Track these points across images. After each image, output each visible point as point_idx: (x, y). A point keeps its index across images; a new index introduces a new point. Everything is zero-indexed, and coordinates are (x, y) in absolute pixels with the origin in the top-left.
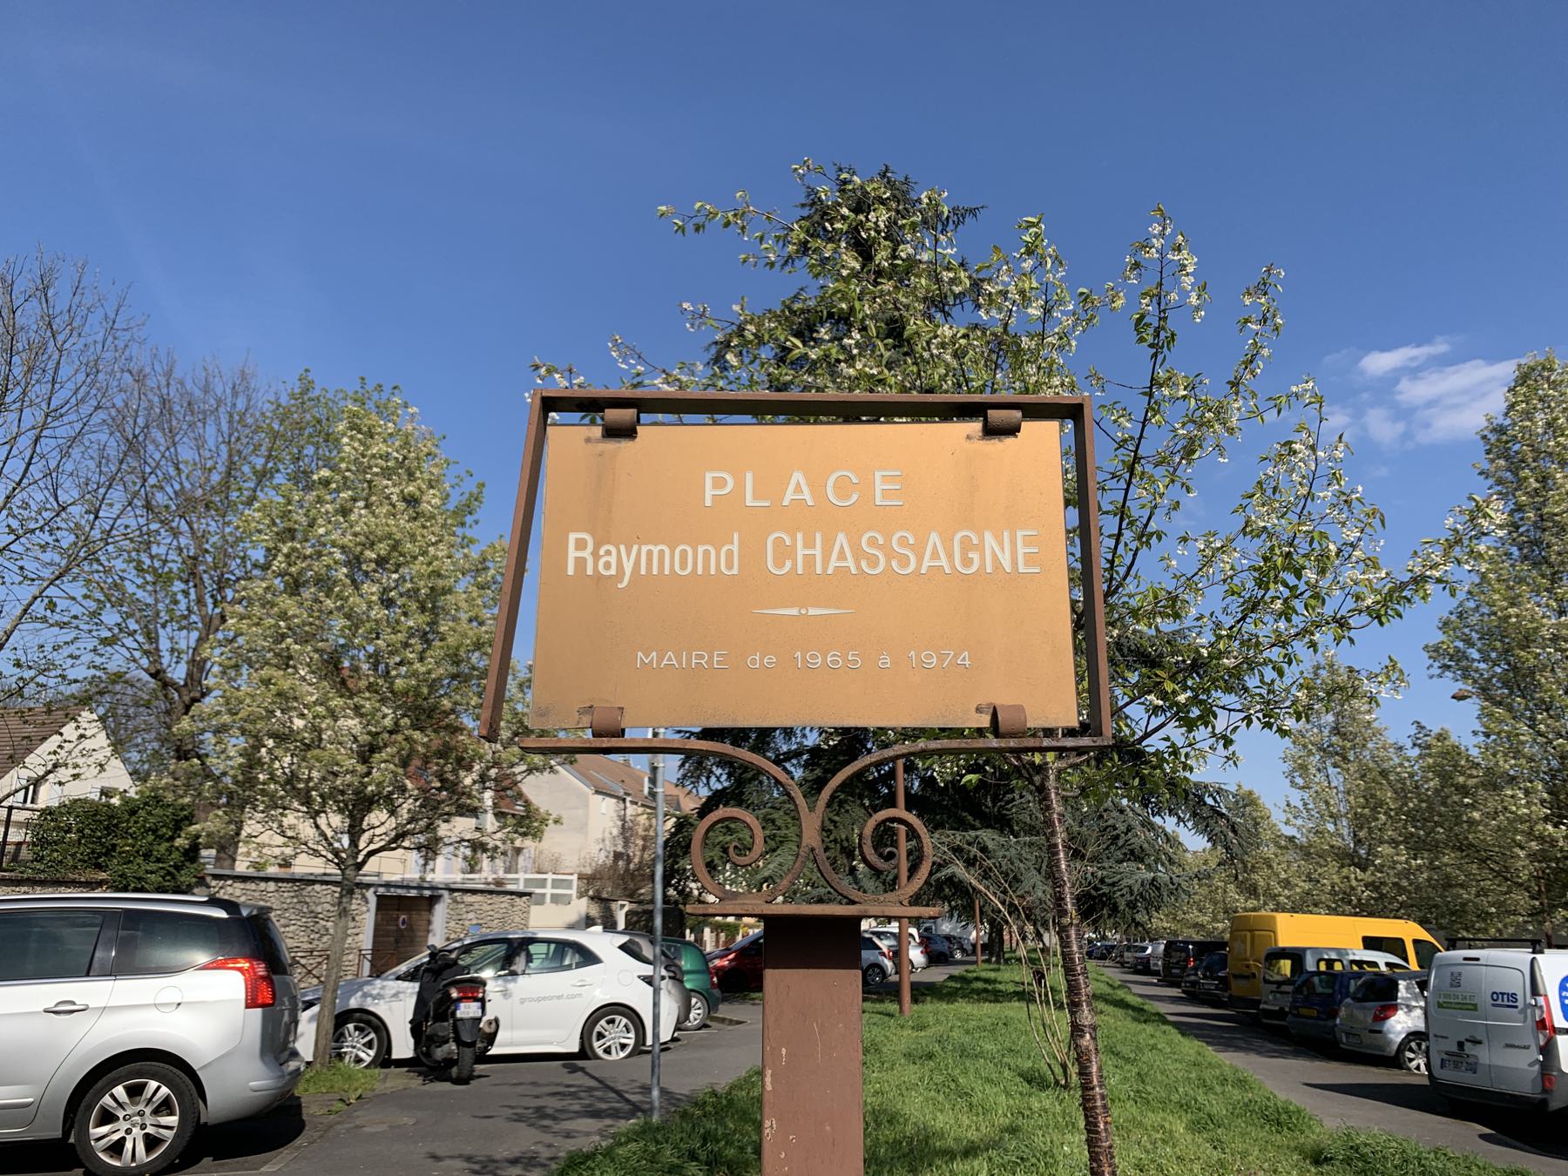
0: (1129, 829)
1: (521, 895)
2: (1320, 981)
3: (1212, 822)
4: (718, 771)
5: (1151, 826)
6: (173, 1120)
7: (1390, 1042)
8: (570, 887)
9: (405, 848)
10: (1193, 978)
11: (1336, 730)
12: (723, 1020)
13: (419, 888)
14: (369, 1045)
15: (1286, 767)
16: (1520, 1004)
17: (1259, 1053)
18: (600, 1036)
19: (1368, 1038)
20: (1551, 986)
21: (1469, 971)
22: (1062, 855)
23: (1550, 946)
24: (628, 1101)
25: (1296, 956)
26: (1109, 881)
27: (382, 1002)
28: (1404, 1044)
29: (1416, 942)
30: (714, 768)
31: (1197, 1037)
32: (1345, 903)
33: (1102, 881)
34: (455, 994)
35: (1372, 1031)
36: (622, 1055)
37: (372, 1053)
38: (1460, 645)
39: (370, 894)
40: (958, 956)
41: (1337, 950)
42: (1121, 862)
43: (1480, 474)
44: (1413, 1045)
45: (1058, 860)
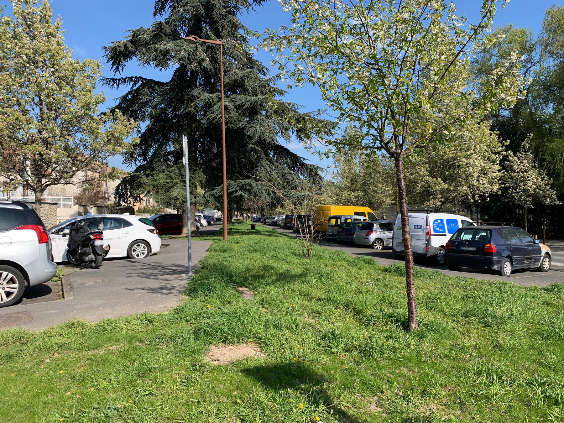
0: (294, 179)
3: (315, 177)
4: (140, 158)
6: (16, 285)
7: (370, 242)
8: (71, 201)
16: (422, 228)
17: (331, 246)
19: (364, 240)
20: (431, 223)
22: (402, 181)
25: (337, 218)
28: (374, 242)
29: (368, 213)
30: (138, 157)
32: (348, 202)
34: (92, 237)
35: (365, 238)
36: (143, 256)
40: (212, 222)
44: (377, 242)
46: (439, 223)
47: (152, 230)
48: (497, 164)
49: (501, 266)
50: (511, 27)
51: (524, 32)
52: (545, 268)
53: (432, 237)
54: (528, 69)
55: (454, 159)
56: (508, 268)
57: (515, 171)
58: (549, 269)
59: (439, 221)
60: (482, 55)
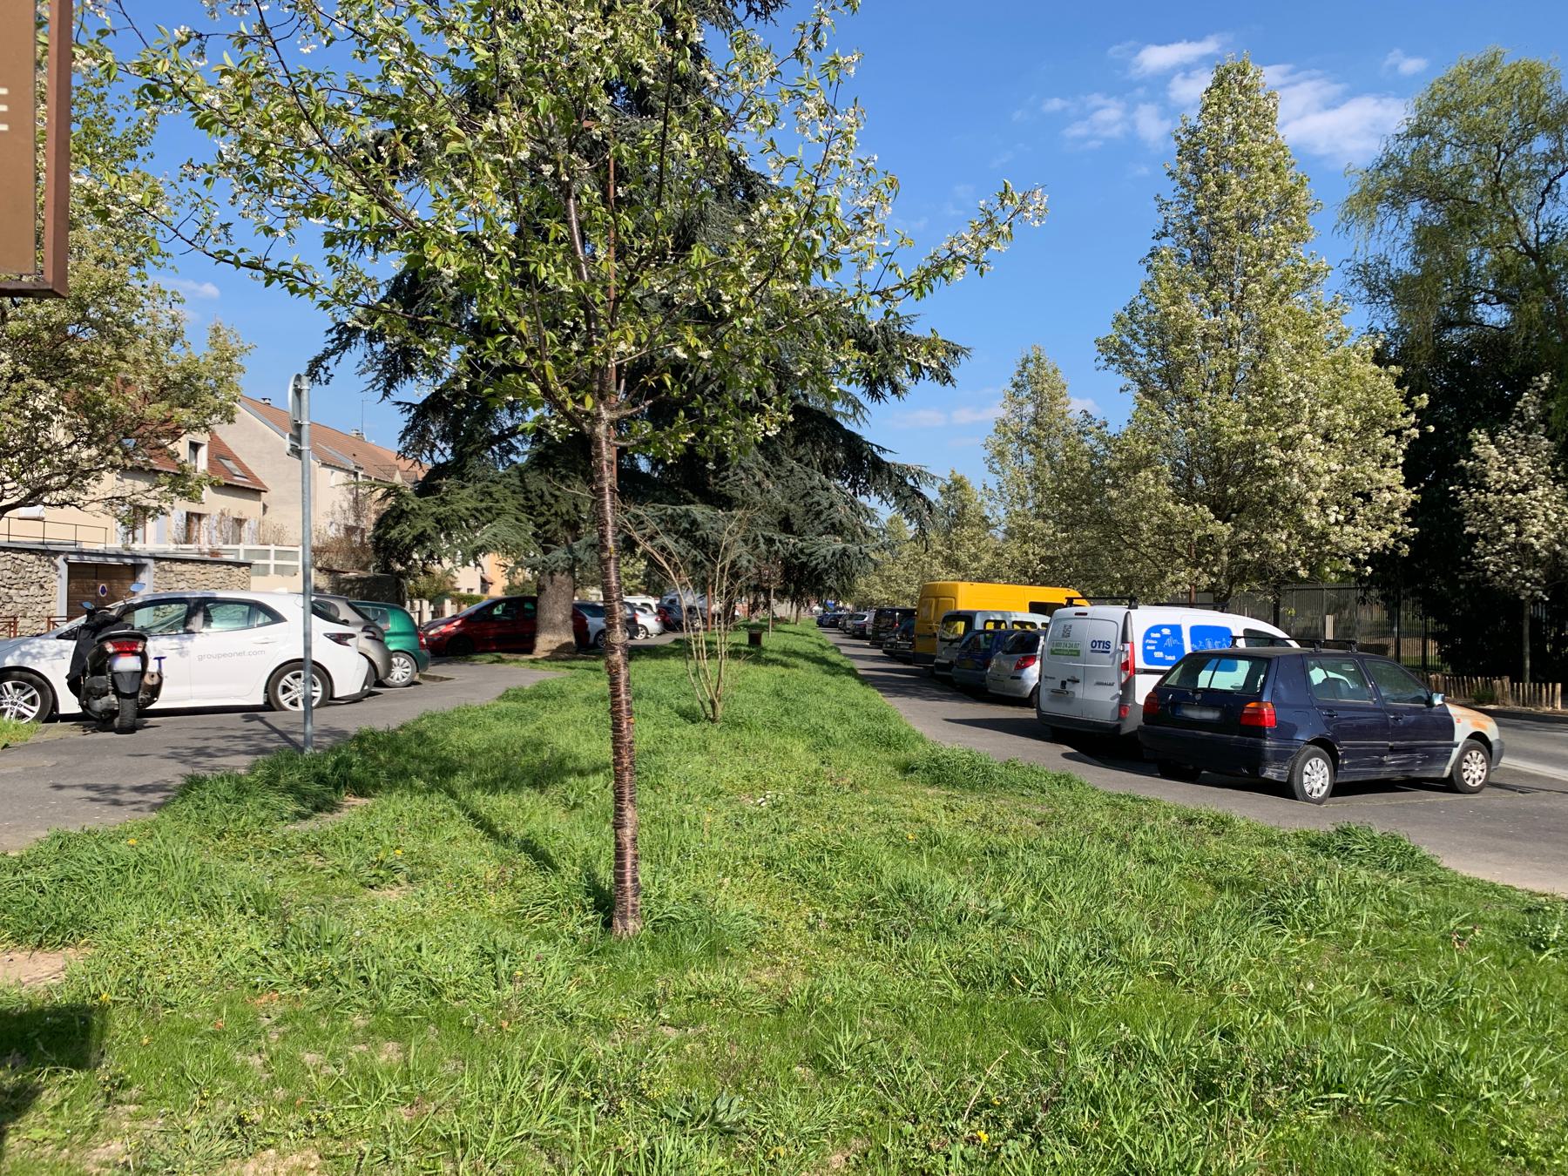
1: (239, 565)
2: (986, 638)
3: (910, 501)
4: (442, 446)
5: (852, 504)
7: (1025, 687)
8: (297, 559)
9: (45, 504)
10: (893, 640)
11: (1035, 421)
12: (434, 678)
13: (118, 556)
14: (32, 701)
15: (987, 454)
16: (1112, 650)
17: (922, 697)
18: (286, 689)
19: (1009, 683)
20: (1137, 636)
21: (1078, 624)
22: (608, 497)
23: (1146, 603)
24: (290, 741)
25: (968, 618)
26: (807, 551)
27: (42, 660)
30: (438, 442)
31: (874, 686)
33: (801, 551)
34: (110, 648)
35: (1013, 678)
37: (36, 709)
38: (1128, 340)
39: (59, 561)
41: (1002, 613)
42: (820, 535)
43: (1169, 174)
45: (604, 502)
46: (1164, 637)
47: (340, 635)
48: (1395, 467)
49: (1293, 767)
50: (1499, 56)
51: (1532, 73)
52: (1470, 783)
53: (1138, 677)
54: (1551, 181)
55: (1249, 448)
56: (1316, 776)
57: (1488, 490)
58: (1488, 783)
59: (1166, 631)
60: (1414, 144)
